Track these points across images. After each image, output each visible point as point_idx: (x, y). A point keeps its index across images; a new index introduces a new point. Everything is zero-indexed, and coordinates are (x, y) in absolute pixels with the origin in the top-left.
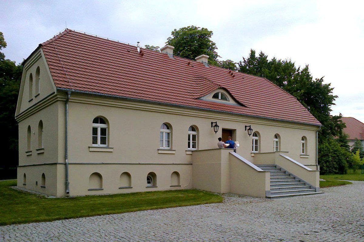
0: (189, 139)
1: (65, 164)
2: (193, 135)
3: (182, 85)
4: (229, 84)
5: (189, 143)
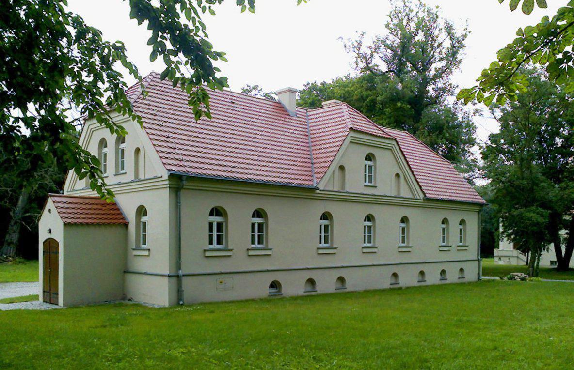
0: (253, 231)
1: (178, 276)
2: (325, 226)
3: (272, 156)
4: (236, 132)
5: (253, 237)
